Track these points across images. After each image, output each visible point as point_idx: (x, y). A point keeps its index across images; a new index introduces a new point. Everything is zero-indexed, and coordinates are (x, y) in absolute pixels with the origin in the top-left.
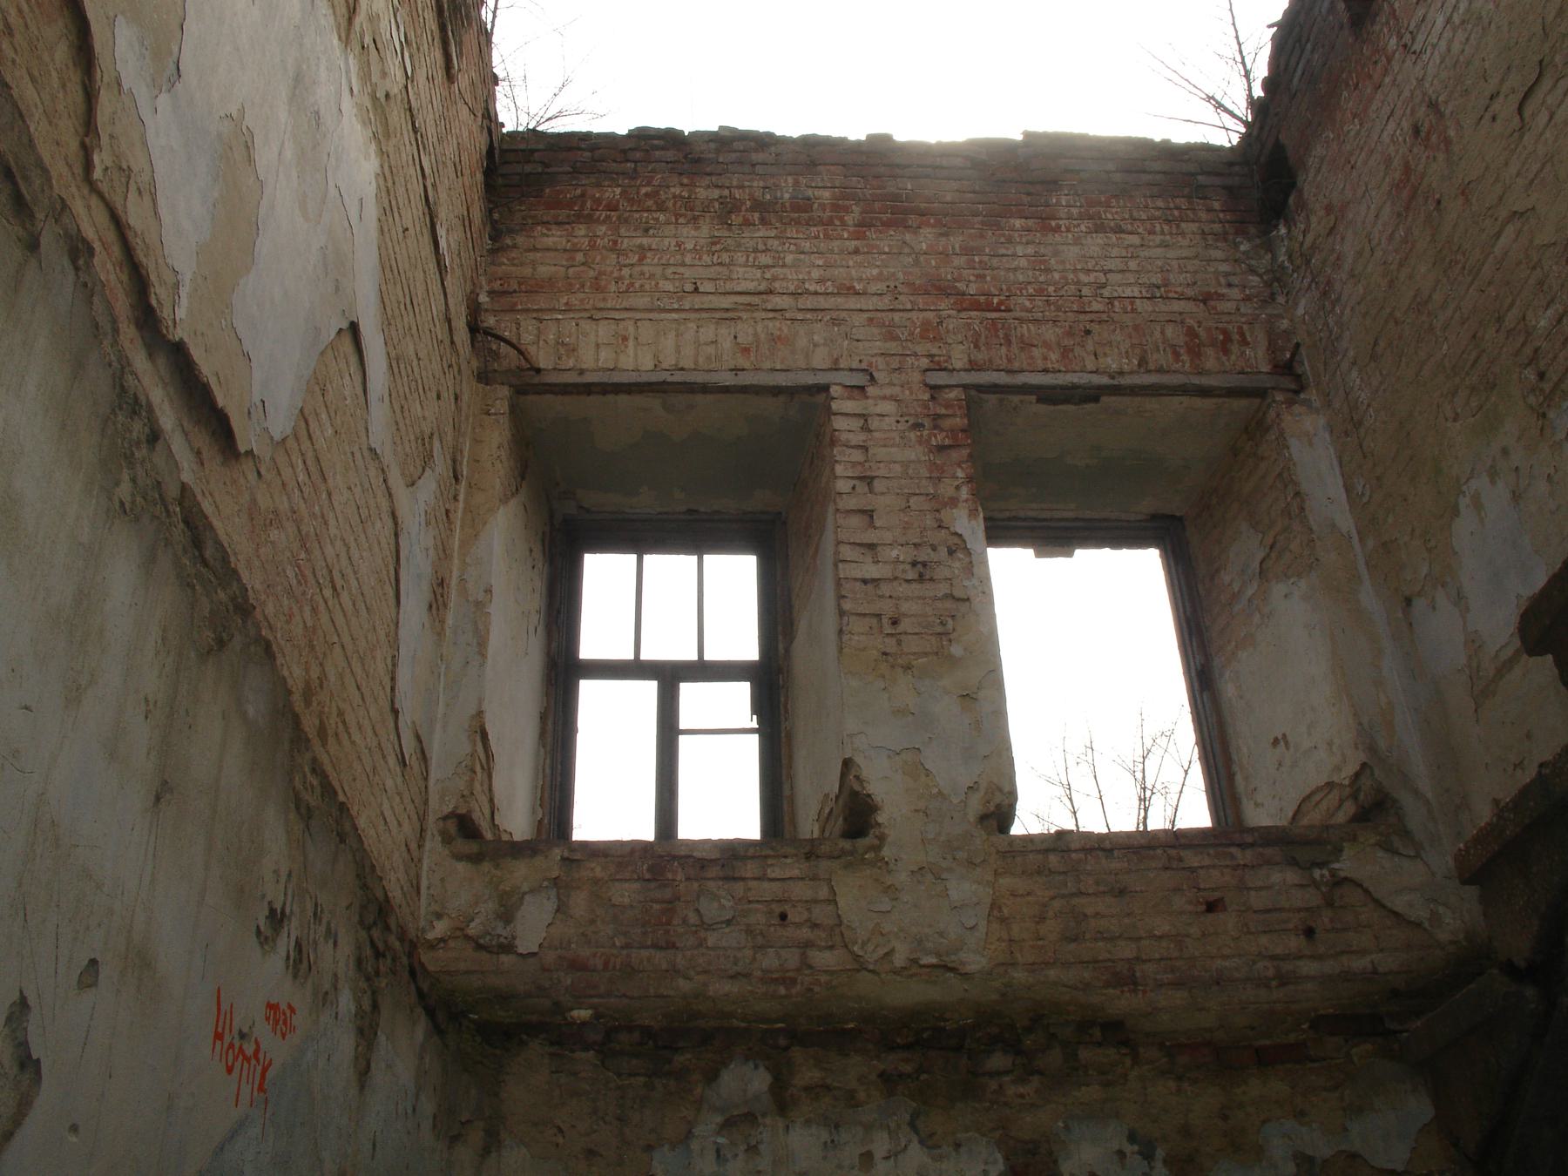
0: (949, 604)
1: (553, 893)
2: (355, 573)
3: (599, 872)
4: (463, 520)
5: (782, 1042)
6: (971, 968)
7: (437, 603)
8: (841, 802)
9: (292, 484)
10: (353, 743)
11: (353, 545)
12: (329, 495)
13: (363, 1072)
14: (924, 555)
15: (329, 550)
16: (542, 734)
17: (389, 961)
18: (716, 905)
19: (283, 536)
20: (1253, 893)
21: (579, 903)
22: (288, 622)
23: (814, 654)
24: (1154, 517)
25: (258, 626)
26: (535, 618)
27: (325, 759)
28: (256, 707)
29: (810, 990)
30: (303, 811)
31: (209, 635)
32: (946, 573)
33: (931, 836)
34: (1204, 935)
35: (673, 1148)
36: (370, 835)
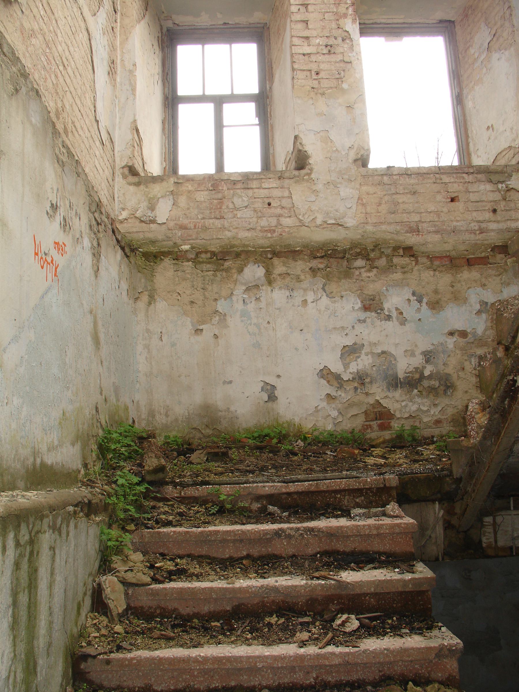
0: (342, 65)
1: (171, 197)
2: (73, 58)
3: (190, 188)
4: (120, 31)
5: (269, 256)
6: (348, 225)
7: (112, 72)
8: (294, 154)
9: (38, 16)
10: (80, 135)
11: (70, 45)
12: (56, 21)
13: (97, 271)
14: (331, 41)
15: (60, 48)
16: (163, 129)
17: (103, 226)
18: (240, 200)
19: (38, 42)
20: (471, 194)
21: (183, 201)
22: (45, 82)
23: (282, 86)
24: (441, 21)
25: (31, 82)
26: (157, 77)
27: (68, 142)
28: (36, 119)
29: (281, 234)
30: (61, 163)
31: (11, 87)
32: (341, 50)
33: (333, 169)
34: (449, 211)
35: (225, 300)
36: (91, 177)
